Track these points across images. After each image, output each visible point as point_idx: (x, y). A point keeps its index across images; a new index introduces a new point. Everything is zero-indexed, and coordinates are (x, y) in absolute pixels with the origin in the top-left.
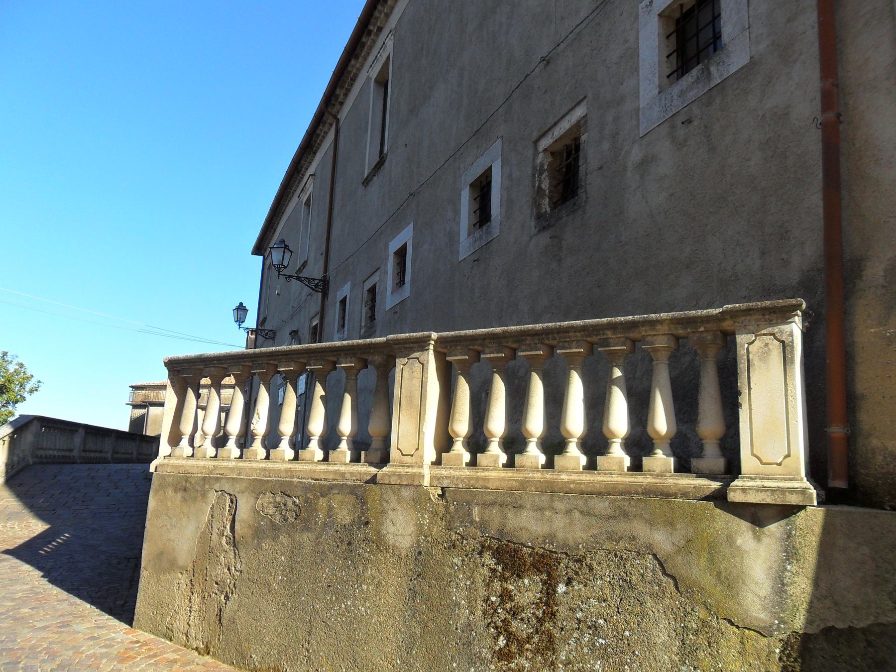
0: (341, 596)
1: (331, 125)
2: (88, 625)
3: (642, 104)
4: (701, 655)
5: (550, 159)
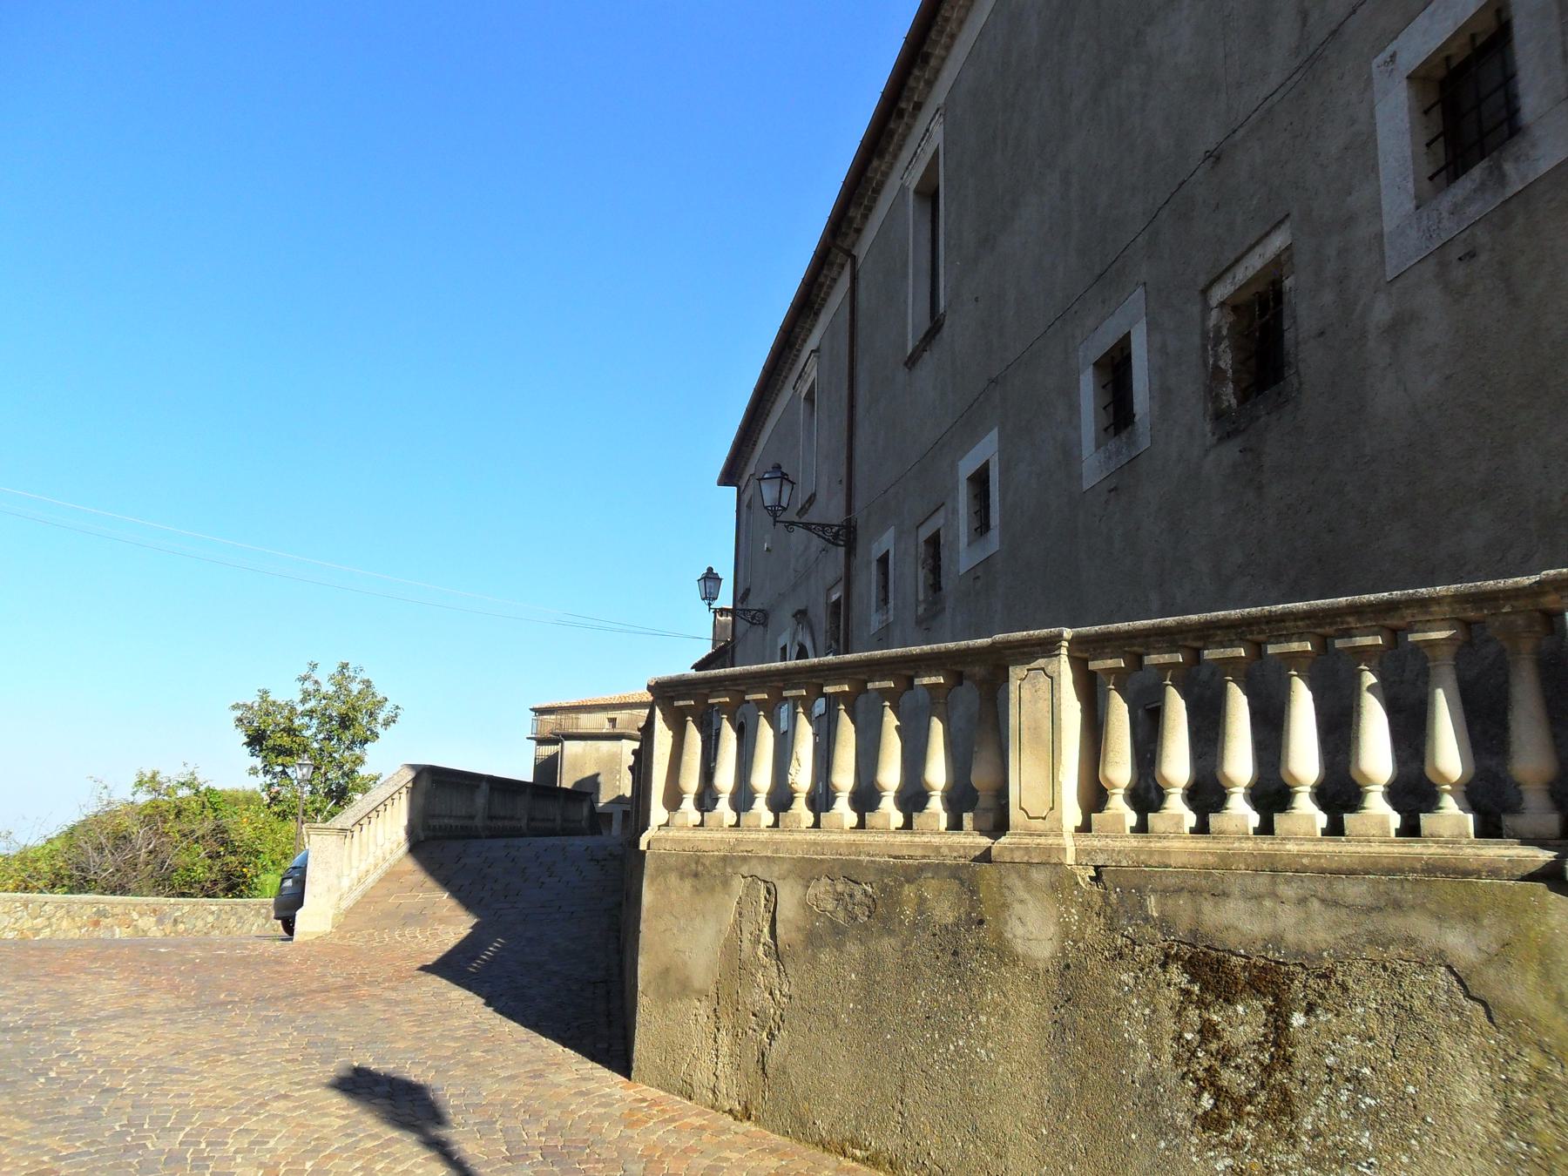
0: (947, 1033)
1: (842, 266)
2: (569, 1076)
3: (1389, 224)
4: (1538, 1123)
5: (1231, 318)
